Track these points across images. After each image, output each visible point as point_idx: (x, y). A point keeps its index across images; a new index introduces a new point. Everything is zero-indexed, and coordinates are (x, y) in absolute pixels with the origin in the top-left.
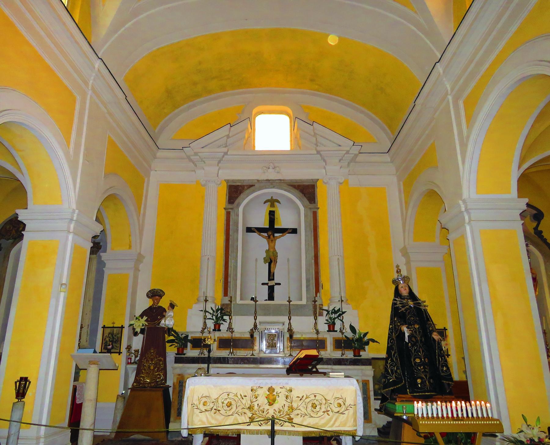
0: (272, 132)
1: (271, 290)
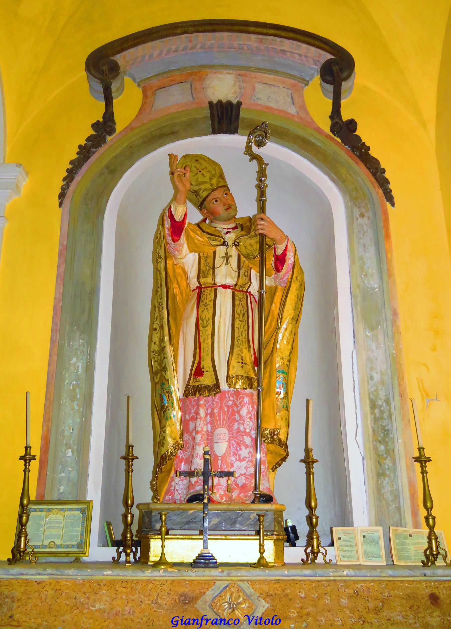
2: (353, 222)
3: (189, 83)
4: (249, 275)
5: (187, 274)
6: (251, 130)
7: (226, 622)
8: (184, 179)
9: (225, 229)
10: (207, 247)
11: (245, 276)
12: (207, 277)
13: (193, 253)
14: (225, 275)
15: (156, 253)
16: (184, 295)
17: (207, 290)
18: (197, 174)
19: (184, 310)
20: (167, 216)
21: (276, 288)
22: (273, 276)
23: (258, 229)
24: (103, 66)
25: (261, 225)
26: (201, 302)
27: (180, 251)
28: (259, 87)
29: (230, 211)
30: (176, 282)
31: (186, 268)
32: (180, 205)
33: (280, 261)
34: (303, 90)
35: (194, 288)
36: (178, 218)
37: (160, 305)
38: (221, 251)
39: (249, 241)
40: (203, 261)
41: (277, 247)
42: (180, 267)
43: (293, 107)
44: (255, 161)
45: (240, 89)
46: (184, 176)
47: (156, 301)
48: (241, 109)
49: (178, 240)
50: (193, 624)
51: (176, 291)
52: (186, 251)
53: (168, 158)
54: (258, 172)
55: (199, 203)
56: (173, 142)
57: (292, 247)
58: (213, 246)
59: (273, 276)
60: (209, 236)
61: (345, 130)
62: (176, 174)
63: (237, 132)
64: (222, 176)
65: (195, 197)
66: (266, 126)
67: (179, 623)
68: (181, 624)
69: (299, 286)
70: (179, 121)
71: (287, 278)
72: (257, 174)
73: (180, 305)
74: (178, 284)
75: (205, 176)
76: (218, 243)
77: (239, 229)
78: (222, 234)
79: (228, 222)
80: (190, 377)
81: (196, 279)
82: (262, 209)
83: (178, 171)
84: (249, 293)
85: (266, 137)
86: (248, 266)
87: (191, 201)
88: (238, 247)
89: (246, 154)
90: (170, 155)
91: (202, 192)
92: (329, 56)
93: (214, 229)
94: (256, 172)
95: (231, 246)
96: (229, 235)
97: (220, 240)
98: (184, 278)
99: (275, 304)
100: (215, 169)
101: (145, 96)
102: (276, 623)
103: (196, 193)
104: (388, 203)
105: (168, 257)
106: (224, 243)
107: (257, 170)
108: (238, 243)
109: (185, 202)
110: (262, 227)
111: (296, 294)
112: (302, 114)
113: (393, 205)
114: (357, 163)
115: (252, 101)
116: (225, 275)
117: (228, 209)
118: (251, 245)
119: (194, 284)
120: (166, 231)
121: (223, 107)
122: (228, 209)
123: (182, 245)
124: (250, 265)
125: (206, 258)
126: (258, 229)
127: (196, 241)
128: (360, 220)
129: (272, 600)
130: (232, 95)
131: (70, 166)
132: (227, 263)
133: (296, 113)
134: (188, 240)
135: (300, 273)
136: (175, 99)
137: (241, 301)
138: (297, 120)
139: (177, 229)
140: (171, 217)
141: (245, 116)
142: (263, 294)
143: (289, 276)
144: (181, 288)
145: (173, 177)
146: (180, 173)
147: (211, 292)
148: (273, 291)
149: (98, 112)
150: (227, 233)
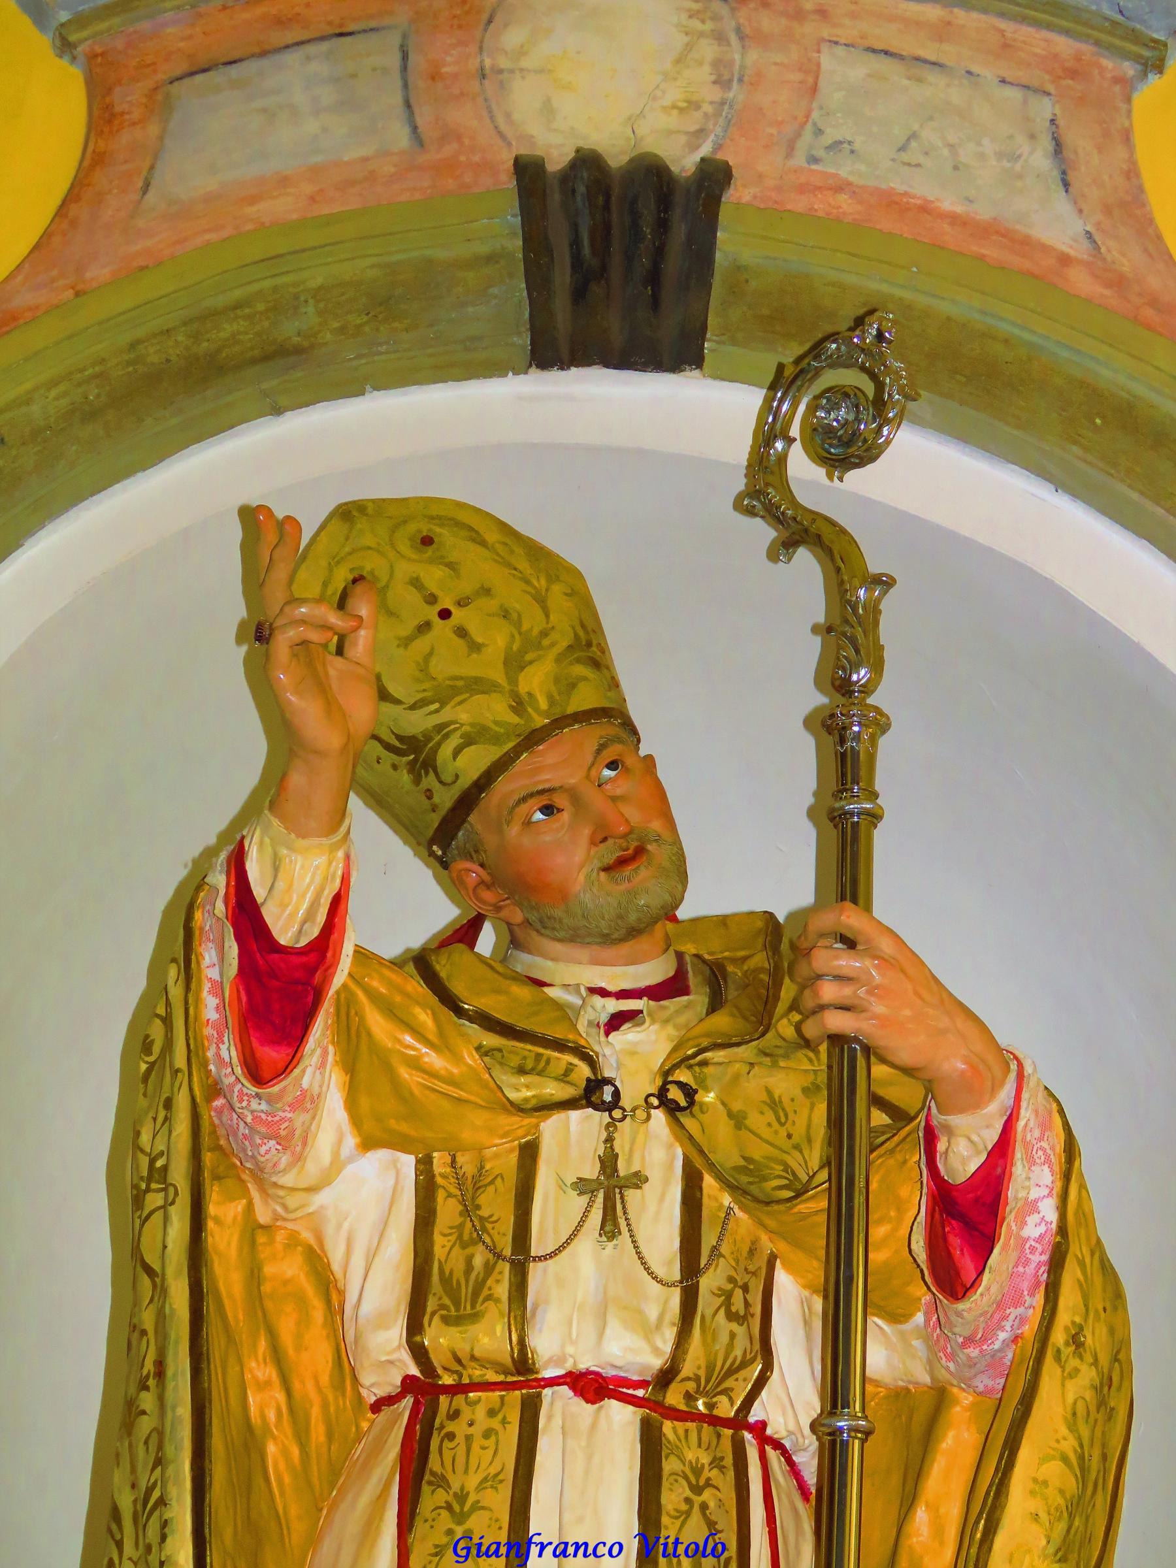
0: (1098, 421)
1: (909, 164)
3: (395, 39)
4: (757, 1309)
5: (341, 1293)
6: (788, 359)
7: (590, 1550)
8: (335, 667)
9: (603, 993)
10: (479, 1118)
11: (731, 1316)
12: (475, 1317)
13: (381, 1155)
14: (597, 1305)
15: (137, 1148)
16: (318, 1433)
17: (472, 1404)
18: (424, 627)
19: (314, 1539)
20: (215, 910)
21: (940, 1397)
22: (920, 1318)
23: (822, 1008)
25: (839, 978)
26: (426, 1489)
27: (294, 1143)
28: (842, 71)
29: (642, 874)
30: (263, 1344)
31: (336, 1257)
32: (302, 835)
33: (967, 1217)
34: (1128, 100)
35: (381, 1392)
36: (290, 922)
37: (151, 1504)
39: (755, 1084)
40: (447, 1211)
41: (949, 1131)
42: (293, 1240)
43: (1061, 204)
44: (803, 555)
45: (722, 82)
46: (340, 651)
47: (119, 1477)
48: (725, 214)
49: (286, 1069)
50: (575, 1556)
51: (265, 1406)
52: (339, 1142)
53: (235, 532)
54: (826, 630)
55: (435, 820)
56: (278, 411)
57: (1045, 1126)
58: (518, 1109)
59: (920, 1318)
60: (491, 1040)
62: (283, 641)
64: (589, 648)
65: (405, 778)
66: (880, 336)
67: (474, 1551)
68: (478, 1556)
69: (1089, 1395)
70: (317, 279)
71: (1015, 1339)
72: (817, 641)
73: (291, 1507)
74: (277, 1355)
75: (475, 647)
76: (553, 1090)
77: (698, 998)
78: (582, 1026)
79: (625, 949)
81: (396, 1332)
82: (846, 865)
83: (303, 622)
84: (759, 1429)
85: (879, 404)
86: (752, 1252)
87: (379, 801)
88: (685, 1119)
89: (750, 512)
90: (252, 518)
91: (457, 753)
93: (524, 992)
94: (815, 629)
95: (641, 1115)
96: (626, 1036)
97: (570, 1069)
98: (318, 1314)
99: (933, 1509)
100: (541, 601)
101: (103, 118)
102: (713, 1553)
103: (417, 753)
105: (217, 1178)
106: (595, 1093)
107: (821, 619)
108: (689, 1093)
109: (341, 813)
110: (849, 993)
111: (1069, 1445)
112: (1126, 256)
115: (799, 160)
116: (597, 1305)
117: (622, 862)
118: (774, 1104)
119: (385, 1358)
120: (210, 1008)
121: (608, 197)
122: (622, 862)
123: (307, 1102)
124: (767, 1244)
125: (471, 1189)
126: (822, 1008)
127: (404, 1073)
130: (672, 121)
132: (610, 1227)
133: (1086, 244)
134: (350, 1066)
135: (1097, 1303)
137: (697, 1490)
138: (1080, 280)
139: (281, 992)
140: (246, 914)
141: (748, 256)
142: (845, 1444)
143: (1023, 1321)
144: (296, 1386)
145: (267, 656)
146: (315, 636)
147: (495, 1423)
148: (920, 1418)
150: (616, 1022)
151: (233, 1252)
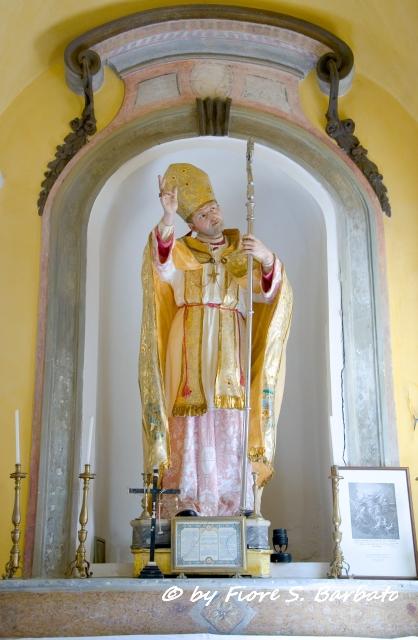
2: (347, 235)
24: (78, 56)
38: (206, 267)
61: (340, 129)
63: (226, 134)
80: (177, 397)
92: (327, 50)
96: (216, 251)
104: (384, 213)
106: (211, 260)
113: (389, 215)
114: (351, 168)
128: (355, 232)
129: (260, 608)
131: (49, 170)
136: (159, 94)
141: (235, 115)
149: (76, 112)
150: (214, 249)
151: (392, 302)
